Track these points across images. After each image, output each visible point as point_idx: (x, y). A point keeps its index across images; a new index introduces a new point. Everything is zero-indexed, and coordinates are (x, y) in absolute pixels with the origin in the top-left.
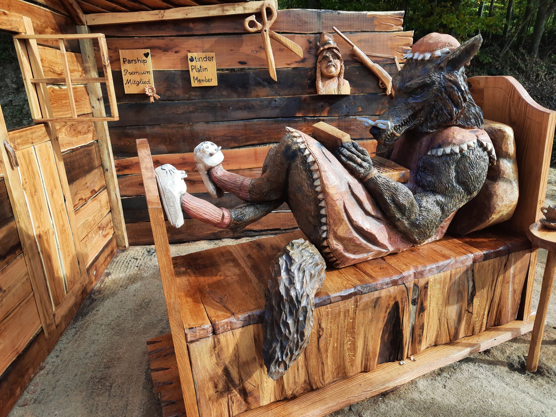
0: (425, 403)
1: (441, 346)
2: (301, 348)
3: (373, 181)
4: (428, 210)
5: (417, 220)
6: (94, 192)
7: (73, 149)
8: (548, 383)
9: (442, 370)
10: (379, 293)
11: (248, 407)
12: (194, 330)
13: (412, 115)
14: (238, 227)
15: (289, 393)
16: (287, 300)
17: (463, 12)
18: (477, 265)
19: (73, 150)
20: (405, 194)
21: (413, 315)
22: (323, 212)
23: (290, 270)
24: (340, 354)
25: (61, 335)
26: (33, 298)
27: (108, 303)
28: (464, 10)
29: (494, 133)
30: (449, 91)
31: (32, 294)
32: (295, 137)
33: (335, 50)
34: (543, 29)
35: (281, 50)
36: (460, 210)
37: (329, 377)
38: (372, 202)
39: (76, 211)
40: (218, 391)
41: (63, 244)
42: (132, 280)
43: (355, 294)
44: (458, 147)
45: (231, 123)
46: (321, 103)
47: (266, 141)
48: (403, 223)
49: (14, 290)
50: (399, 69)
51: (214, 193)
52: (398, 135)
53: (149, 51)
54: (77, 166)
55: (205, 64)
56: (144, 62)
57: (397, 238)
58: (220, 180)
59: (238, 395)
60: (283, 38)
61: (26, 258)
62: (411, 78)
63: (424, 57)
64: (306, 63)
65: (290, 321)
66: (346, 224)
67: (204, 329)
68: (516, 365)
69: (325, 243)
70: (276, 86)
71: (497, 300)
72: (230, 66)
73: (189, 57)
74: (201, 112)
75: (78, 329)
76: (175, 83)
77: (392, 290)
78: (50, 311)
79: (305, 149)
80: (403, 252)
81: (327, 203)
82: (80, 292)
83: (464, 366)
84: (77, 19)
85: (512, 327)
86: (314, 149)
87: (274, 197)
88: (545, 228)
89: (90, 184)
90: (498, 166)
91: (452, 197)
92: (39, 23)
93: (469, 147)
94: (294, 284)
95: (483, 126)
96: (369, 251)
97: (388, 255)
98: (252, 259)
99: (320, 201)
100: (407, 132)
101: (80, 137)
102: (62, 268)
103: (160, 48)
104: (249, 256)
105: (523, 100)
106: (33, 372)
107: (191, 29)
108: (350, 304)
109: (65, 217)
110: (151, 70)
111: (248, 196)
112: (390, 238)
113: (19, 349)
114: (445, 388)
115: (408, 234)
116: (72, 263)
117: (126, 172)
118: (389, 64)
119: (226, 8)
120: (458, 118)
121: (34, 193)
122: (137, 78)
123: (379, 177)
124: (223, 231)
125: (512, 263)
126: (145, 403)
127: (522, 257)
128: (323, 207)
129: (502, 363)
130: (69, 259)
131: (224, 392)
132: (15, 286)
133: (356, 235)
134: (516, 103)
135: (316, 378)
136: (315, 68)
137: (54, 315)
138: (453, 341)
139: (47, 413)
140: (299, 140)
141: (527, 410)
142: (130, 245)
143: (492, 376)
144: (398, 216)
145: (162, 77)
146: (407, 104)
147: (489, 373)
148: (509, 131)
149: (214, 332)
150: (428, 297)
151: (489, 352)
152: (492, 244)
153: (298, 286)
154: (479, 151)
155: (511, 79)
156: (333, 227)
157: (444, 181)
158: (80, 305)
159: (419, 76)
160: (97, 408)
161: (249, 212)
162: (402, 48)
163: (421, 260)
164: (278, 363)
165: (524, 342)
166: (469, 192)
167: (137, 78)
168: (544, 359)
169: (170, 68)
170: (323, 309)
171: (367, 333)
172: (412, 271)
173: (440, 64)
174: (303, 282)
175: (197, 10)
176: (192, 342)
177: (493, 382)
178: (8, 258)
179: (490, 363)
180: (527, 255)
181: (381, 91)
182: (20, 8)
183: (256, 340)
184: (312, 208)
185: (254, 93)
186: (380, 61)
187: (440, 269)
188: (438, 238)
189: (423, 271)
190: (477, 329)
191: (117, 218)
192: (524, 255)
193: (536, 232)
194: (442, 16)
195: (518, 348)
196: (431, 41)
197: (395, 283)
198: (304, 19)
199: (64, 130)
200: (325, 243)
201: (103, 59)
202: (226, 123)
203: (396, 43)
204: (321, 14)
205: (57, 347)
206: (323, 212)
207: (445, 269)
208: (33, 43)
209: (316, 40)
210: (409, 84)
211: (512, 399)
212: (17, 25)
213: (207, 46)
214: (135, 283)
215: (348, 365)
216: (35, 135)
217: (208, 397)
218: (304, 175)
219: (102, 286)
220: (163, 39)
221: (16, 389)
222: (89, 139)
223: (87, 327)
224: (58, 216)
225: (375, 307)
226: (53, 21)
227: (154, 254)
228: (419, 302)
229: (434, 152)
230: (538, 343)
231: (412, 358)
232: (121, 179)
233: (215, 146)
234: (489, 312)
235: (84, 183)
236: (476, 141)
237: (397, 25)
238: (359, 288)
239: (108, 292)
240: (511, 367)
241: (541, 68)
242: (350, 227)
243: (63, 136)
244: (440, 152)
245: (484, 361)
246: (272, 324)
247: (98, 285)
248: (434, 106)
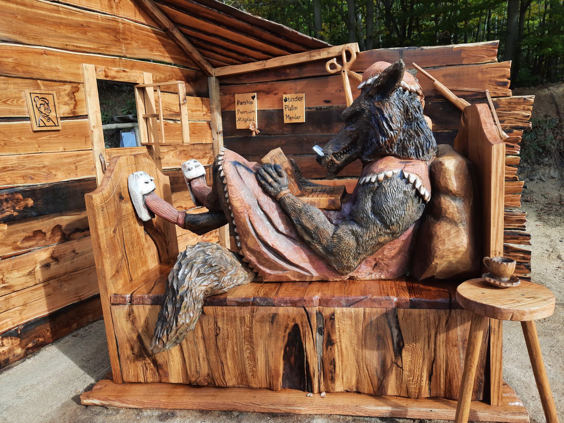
4: (340, 238)
24: (241, 360)
44: (376, 176)
52: (337, 162)
55: (296, 104)
56: (251, 103)
103: (264, 91)
107: (288, 74)
108: (246, 311)
113: (82, 297)
119: (313, 54)
122: (245, 116)
125: (458, 323)
145: (264, 115)
149: (131, 302)
156: (243, 238)
167: (245, 116)
169: (269, 107)
172: (317, 297)
173: (368, 92)
182: (144, 67)
186: (468, 96)
204: (404, 52)
213: (299, 88)
215: (249, 374)
225: (272, 322)
228: (325, 332)
237: (489, 56)
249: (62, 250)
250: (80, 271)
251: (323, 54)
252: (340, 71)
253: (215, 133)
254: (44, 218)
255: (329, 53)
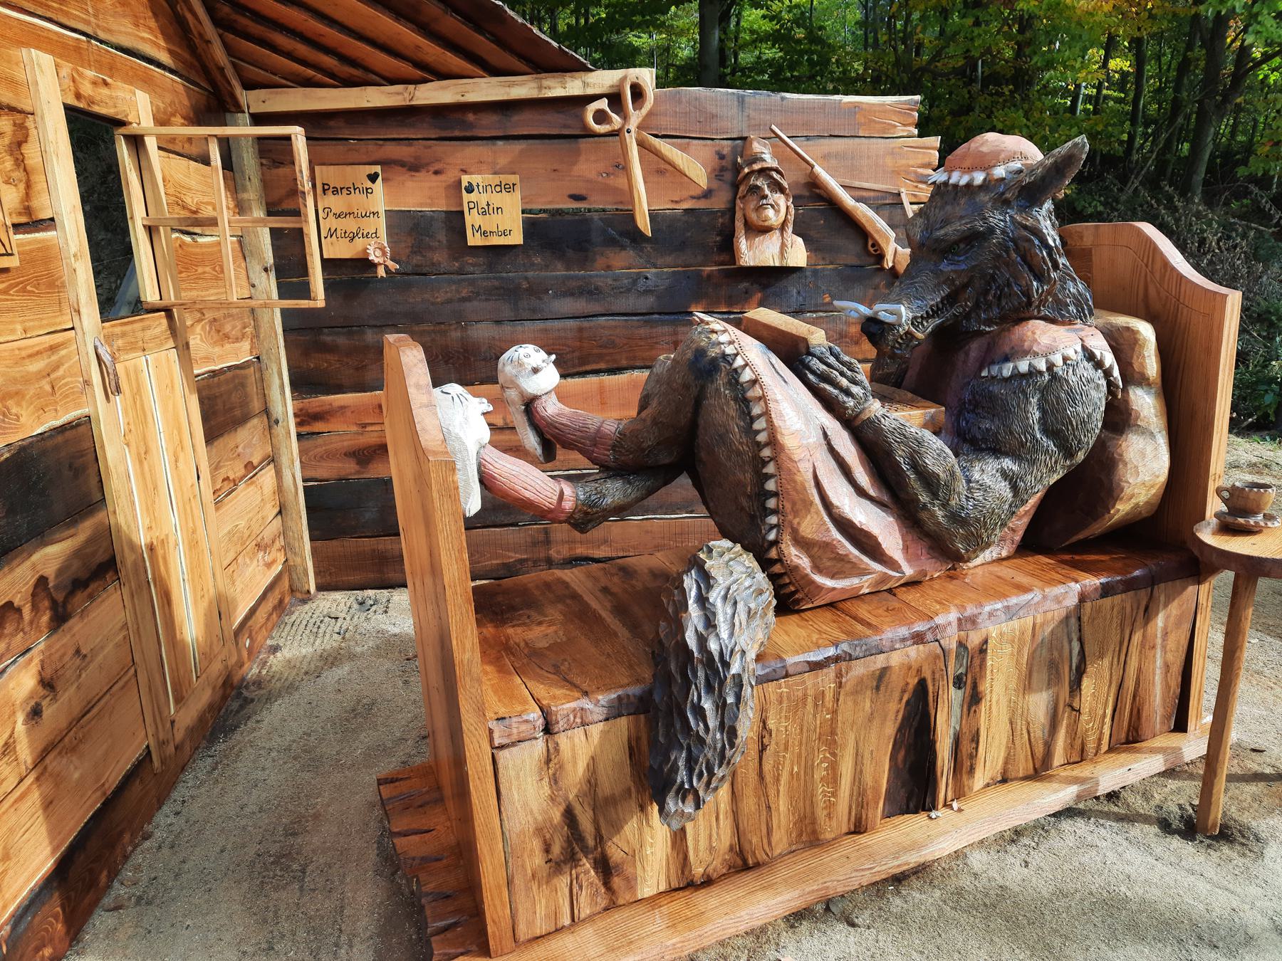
0: (987, 895)
1: (1015, 783)
2: (729, 763)
3: (872, 424)
4: (985, 488)
5: (963, 508)
6: (249, 466)
7: (213, 371)
8: (1244, 855)
9: (1018, 832)
10: (887, 659)
11: (611, 900)
12: (507, 722)
13: (948, 297)
14: (590, 521)
15: (698, 871)
16: (701, 661)
17: (1038, 104)
18: (1088, 605)
19: (214, 373)
20: (938, 453)
21: (956, 710)
22: (771, 485)
23: (707, 599)
24: (805, 791)
25: (183, 769)
26: (133, 680)
27: (279, 708)
28: (1040, 99)
29: (1116, 335)
30: (1024, 245)
31: (132, 671)
32: (713, 332)
33: (775, 175)
34: (1210, 146)
35: (660, 172)
36: (1052, 492)
37: (781, 840)
38: (871, 469)
39: (218, 504)
40: (550, 860)
41: (192, 570)
42: (330, 660)
43: (837, 659)
45: (549, 324)
46: (744, 285)
47: (624, 363)
48: (933, 515)
49: (100, 657)
50: (910, 215)
51: (539, 451)
52: (920, 336)
53: (378, 169)
54: (224, 406)
55: (498, 199)
56: (368, 191)
57: (920, 548)
58: (552, 424)
59: (592, 872)
60: (664, 147)
61: (125, 590)
62: (946, 222)
63: (972, 180)
64: (713, 199)
65: (707, 705)
66: (818, 512)
67: (527, 721)
68: (1176, 824)
69: (773, 554)
70: (648, 247)
71: (1130, 684)
72: (550, 202)
73: (464, 184)
74: (487, 300)
75: (217, 759)
76: (433, 237)
77: (914, 653)
78: (166, 713)
79: (736, 355)
80: (932, 579)
81: (779, 467)
82: (220, 681)
83: (1066, 825)
84: (228, 99)
85: (1164, 745)
86: (756, 359)
87: (665, 459)
88: (1227, 528)
89: (244, 448)
90: (1126, 401)
91: (1033, 462)
92: (161, 105)
93: (1065, 359)
94: (715, 627)
95: (1091, 321)
96: (864, 572)
97: (902, 585)
98: (612, 594)
99: (765, 463)
100: (937, 333)
101: (228, 346)
102: (191, 625)
103: (402, 164)
104: (605, 590)
105: (1173, 269)
106: (131, 842)
107: (472, 126)
108: (826, 679)
109: (198, 513)
110: (381, 209)
111: (610, 456)
112: (906, 549)
114: (1026, 866)
115: (943, 539)
116: (208, 616)
117: (319, 426)
118: (889, 204)
119: (546, 83)
120: (1042, 302)
121: (143, 455)
122: (350, 225)
123: (884, 416)
124: (526, 560)
126: (382, 903)
127: (1181, 592)
128: (772, 476)
129: (1146, 819)
130: (204, 604)
131: (565, 862)
132: (102, 648)
133: (836, 535)
134: (1158, 276)
135: (754, 840)
136: (732, 210)
137: (173, 722)
138: (1040, 771)
139: (168, 924)
140: (723, 338)
141: (1201, 907)
142: (320, 588)
143: (1125, 843)
144: (924, 498)
145: (407, 227)
146: (937, 273)
147: (1119, 838)
148: (1146, 331)
149: (548, 730)
150: (988, 672)
151: (1118, 797)
152: (1119, 565)
153: (724, 634)
154: (1087, 370)
155: (1148, 229)
156: (790, 517)
157: (1017, 428)
158: (219, 711)
159: (961, 218)
160: (276, 912)
161: (614, 492)
162: (916, 173)
163: (970, 595)
164: (682, 794)
165: (1191, 777)
166: (1069, 453)
167: (350, 225)
168: (1233, 809)
169: (421, 205)
170: (771, 687)
171: (861, 744)
172: (953, 616)
173: (1003, 193)
174: (733, 625)
175: (484, 86)
176: (502, 747)
177: (1127, 855)
178: (93, 586)
179: (1120, 818)
180: (1191, 589)
181: (872, 260)
183: (633, 750)
184: (747, 477)
185: (600, 262)
186: (869, 198)
187: (1010, 613)
188: (1004, 554)
189: (975, 616)
190: (1091, 746)
191: (294, 528)
192: (1184, 589)
193: (1207, 535)
194: (992, 112)
195: (1179, 789)
196: (984, 149)
197: (918, 638)
198: (712, 109)
199: (198, 328)
200: (773, 554)
201: (299, 178)
202: (540, 325)
203: (904, 162)
204: (747, 99)
205: (175, 795)
206: (771, 485)
207: (1021, 613)
208: (151, 143)
209: (735, 152)
210: (942, 232)
211: (1169, 887)
212: (126, 108)
213: (502, 161)
214: (337, 666)
215: (821, 814)
216: (149, 333)
217: (529, 871)
218: (732, 409)
219: (264, 672)
220: (410, 145)
221: (101, 872)
222: (240, 353)
223: (238, 756)
224: (185, 510)
225: (878, 688)
226: (186, 102)
227: (374, 608)
228: (969, 682)
229: (995, 370)
230: (1219, 770)
231: (955, 805)
232: (308, 443)
233: (543, 355)
234: (1114, 711)
235: (232, 445)
236: (1079, 349)
237: (904, 125)
238: (845, 647)
239: (278, 685)
240: (1165, 826)
241: (1210, 225)
242: (826, 519)
243: (197, 341)
244: (1007, 370)
245: (1107, 816)
246: (670, 713)
247: (255, 670)
248: (993, 277)
249: (57, 655)
250: (95, 710)
251: (573, 86)
252: (620, 130)
253: (258, 268)
254: (12, 560)
255: (585, 84)
